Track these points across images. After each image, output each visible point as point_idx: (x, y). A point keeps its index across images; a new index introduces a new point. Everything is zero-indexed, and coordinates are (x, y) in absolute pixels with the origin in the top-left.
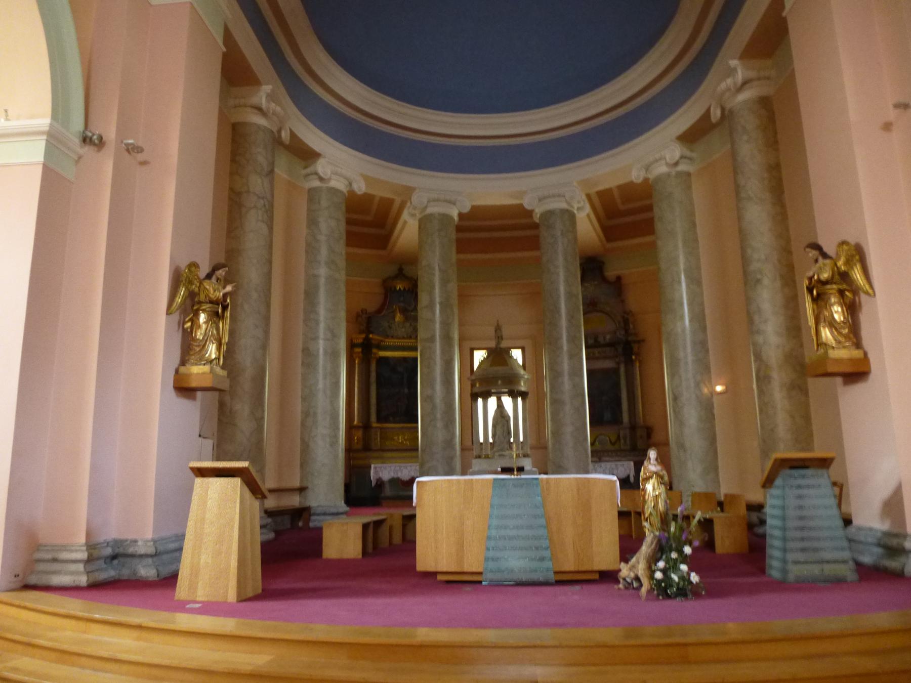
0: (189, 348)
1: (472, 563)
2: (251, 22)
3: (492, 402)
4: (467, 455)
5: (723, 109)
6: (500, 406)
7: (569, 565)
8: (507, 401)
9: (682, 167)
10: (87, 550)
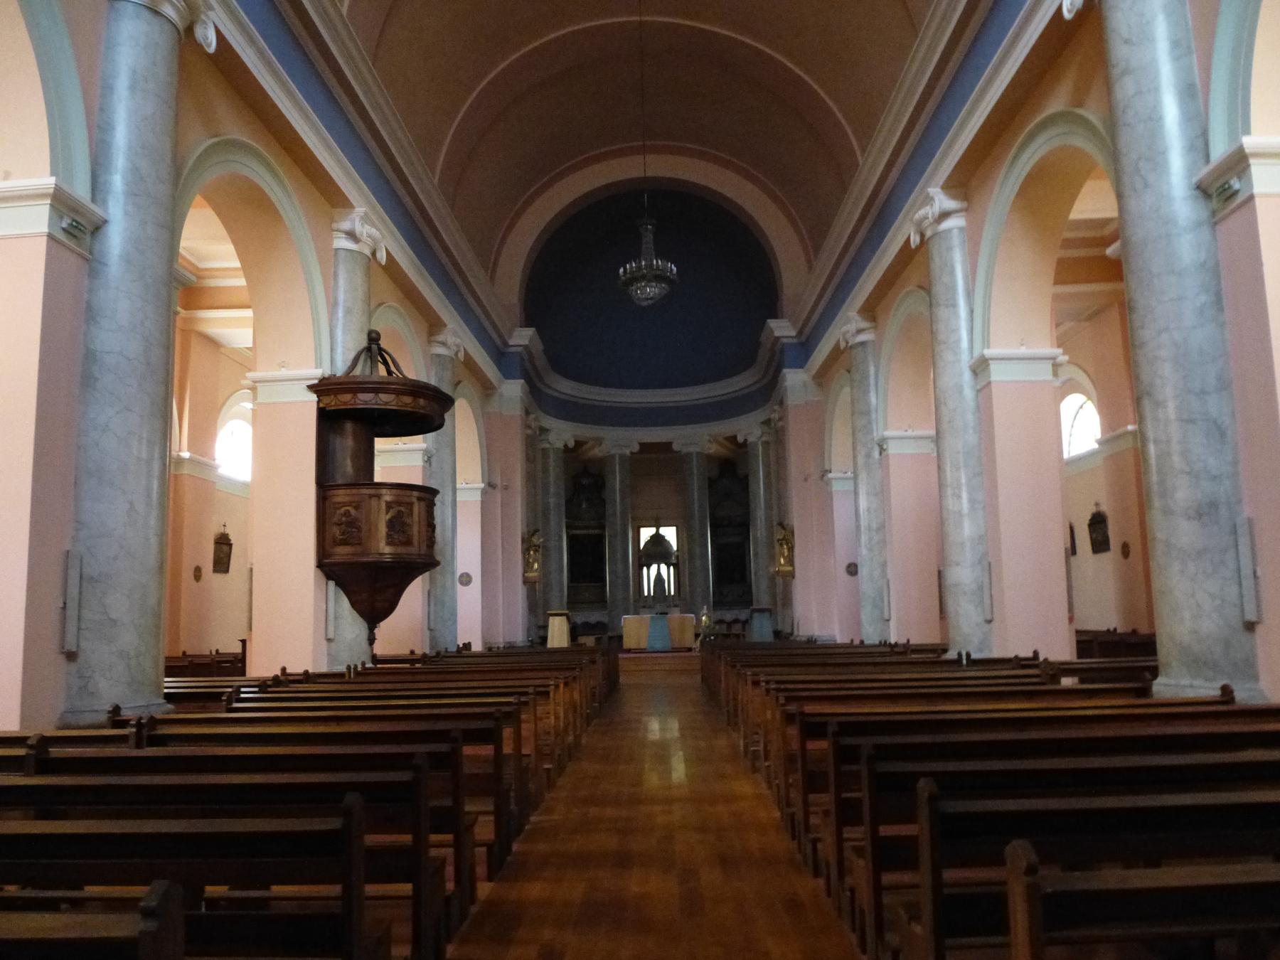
0: (527, 566)
1: (644, 645)
2: (480, 341)
3: (654, 568)
4: (640, 603)
5: (922, 235)
6: (659, 573)
7: (677, 646)
8: (663, 567)
9: (764, 439)
10: (1087, 643)
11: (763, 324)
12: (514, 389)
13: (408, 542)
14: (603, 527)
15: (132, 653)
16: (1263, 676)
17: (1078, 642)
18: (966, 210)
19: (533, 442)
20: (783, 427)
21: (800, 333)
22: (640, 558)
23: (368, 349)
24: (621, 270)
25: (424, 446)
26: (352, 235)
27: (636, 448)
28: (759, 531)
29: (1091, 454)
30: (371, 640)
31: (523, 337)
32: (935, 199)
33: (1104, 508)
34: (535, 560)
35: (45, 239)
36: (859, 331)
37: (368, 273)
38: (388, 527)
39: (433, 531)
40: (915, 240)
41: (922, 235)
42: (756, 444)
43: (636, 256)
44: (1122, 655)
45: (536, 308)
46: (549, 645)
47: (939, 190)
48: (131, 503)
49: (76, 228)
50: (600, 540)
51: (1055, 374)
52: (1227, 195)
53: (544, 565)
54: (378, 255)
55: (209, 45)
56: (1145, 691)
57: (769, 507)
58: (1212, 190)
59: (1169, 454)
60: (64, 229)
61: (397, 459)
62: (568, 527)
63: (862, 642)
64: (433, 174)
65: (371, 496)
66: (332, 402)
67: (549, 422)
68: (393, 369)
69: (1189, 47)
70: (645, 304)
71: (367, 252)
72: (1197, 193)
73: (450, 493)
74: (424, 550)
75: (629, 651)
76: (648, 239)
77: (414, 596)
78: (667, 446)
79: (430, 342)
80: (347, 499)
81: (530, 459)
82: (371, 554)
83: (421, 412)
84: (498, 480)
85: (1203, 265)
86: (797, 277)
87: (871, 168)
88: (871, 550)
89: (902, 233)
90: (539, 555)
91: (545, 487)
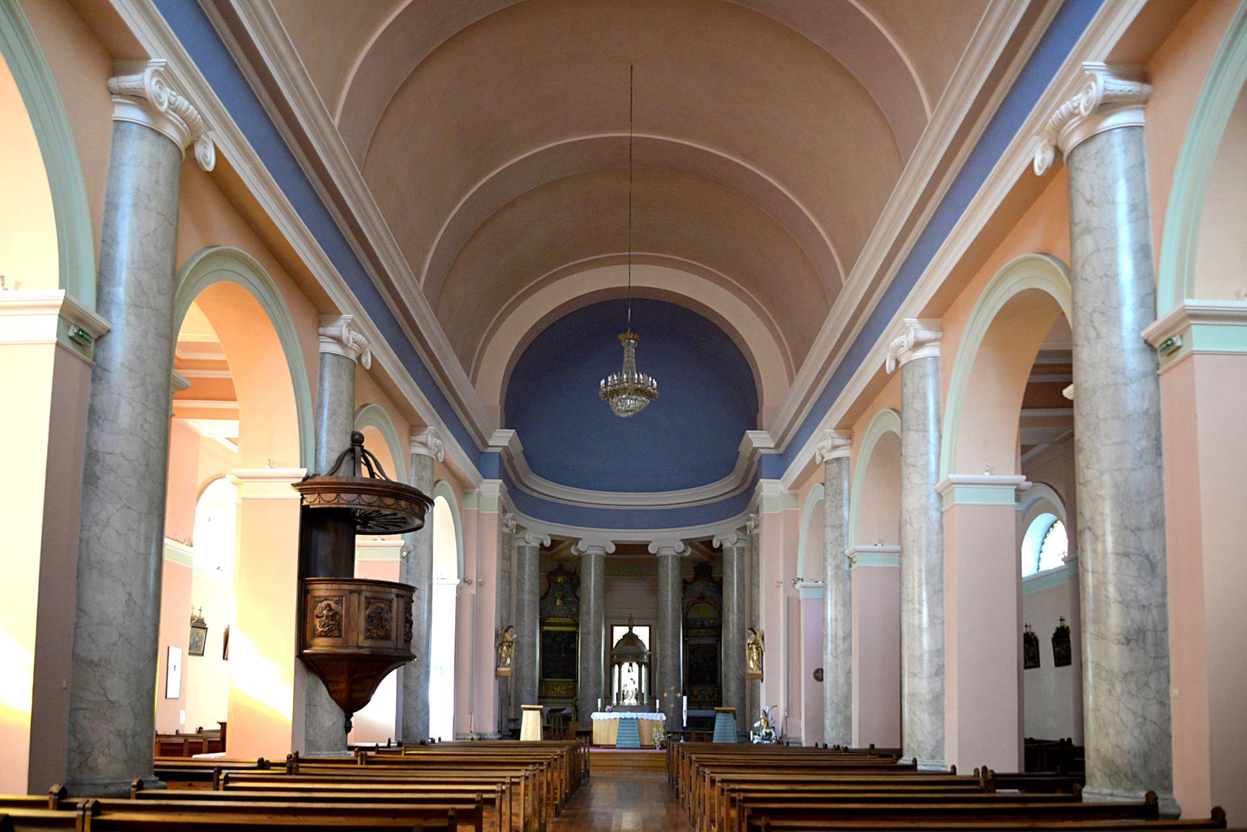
5: (897, 362)
11: (741, 435)
12: (492, 489)
13: (387, 637)
14: (577, 625)
15: (129, 732)
16: (1175, 791)
17: (1027, 749)
18: (940, 340)
19: (507, 541)
20: (758, 535)
21: (777, 446)
22: (612, 657)
23: (352, 450)
24: (603, 382)
25: (402, 542)
26: (338, 340)
27: (612, 549)
28: (730, 634)
29: (1058, 571)
30: (348, 728)
31: (502, 438)
32: (905, 334)
33: (1068, 623)
34: (508, 655)
35: (54, 346)
36: (835, 448)
37: (353, 378)
38: (366, 621)
39: (411, 626)
40: (890, 366)
41: (897, 362)
42: (731, 549)
43: (617, 368)
44: (1054, 762)
45: (515, 412)
46: (522, 739)
47: (915, 320)
48: (130, 594)
49: (81, 338)
50: (574, 635)
51: (1018, 499)
52: (1170, 348)
53: (516, 660)
54: (363, 360)
55: (208, 164)
56: (1079, 798)
57: (741, 611)
58: (1156, 346)
59: (1105, 584)
60: (71, 338)
61: (376, 557)
62: (542, 624)
63: (825, 746)
64: (418, 279)
65: (351, 592)
66: (312, 500)
67: (526, 521)
68: (375, 470)
69: (1146, 212)
70: (625, 415)
71: (353, 356)
72: (1142, 345)
73: (426, 588)
74: (401, 644)
75: (598, 746)
76: (630, 344)
77: (388, 688)
78: (643, 548)
79: (411, 441)
80: (328, 593)
81: (505, 557)
82: (352, 646)
83: (402, 509)
84: (473, 576)
85: (1146, 412)
86: (781, 391)
87: (855, 287)
88: (836, 657)
89: (880, 357)
90: (512, 650)
91: (520, 582)
